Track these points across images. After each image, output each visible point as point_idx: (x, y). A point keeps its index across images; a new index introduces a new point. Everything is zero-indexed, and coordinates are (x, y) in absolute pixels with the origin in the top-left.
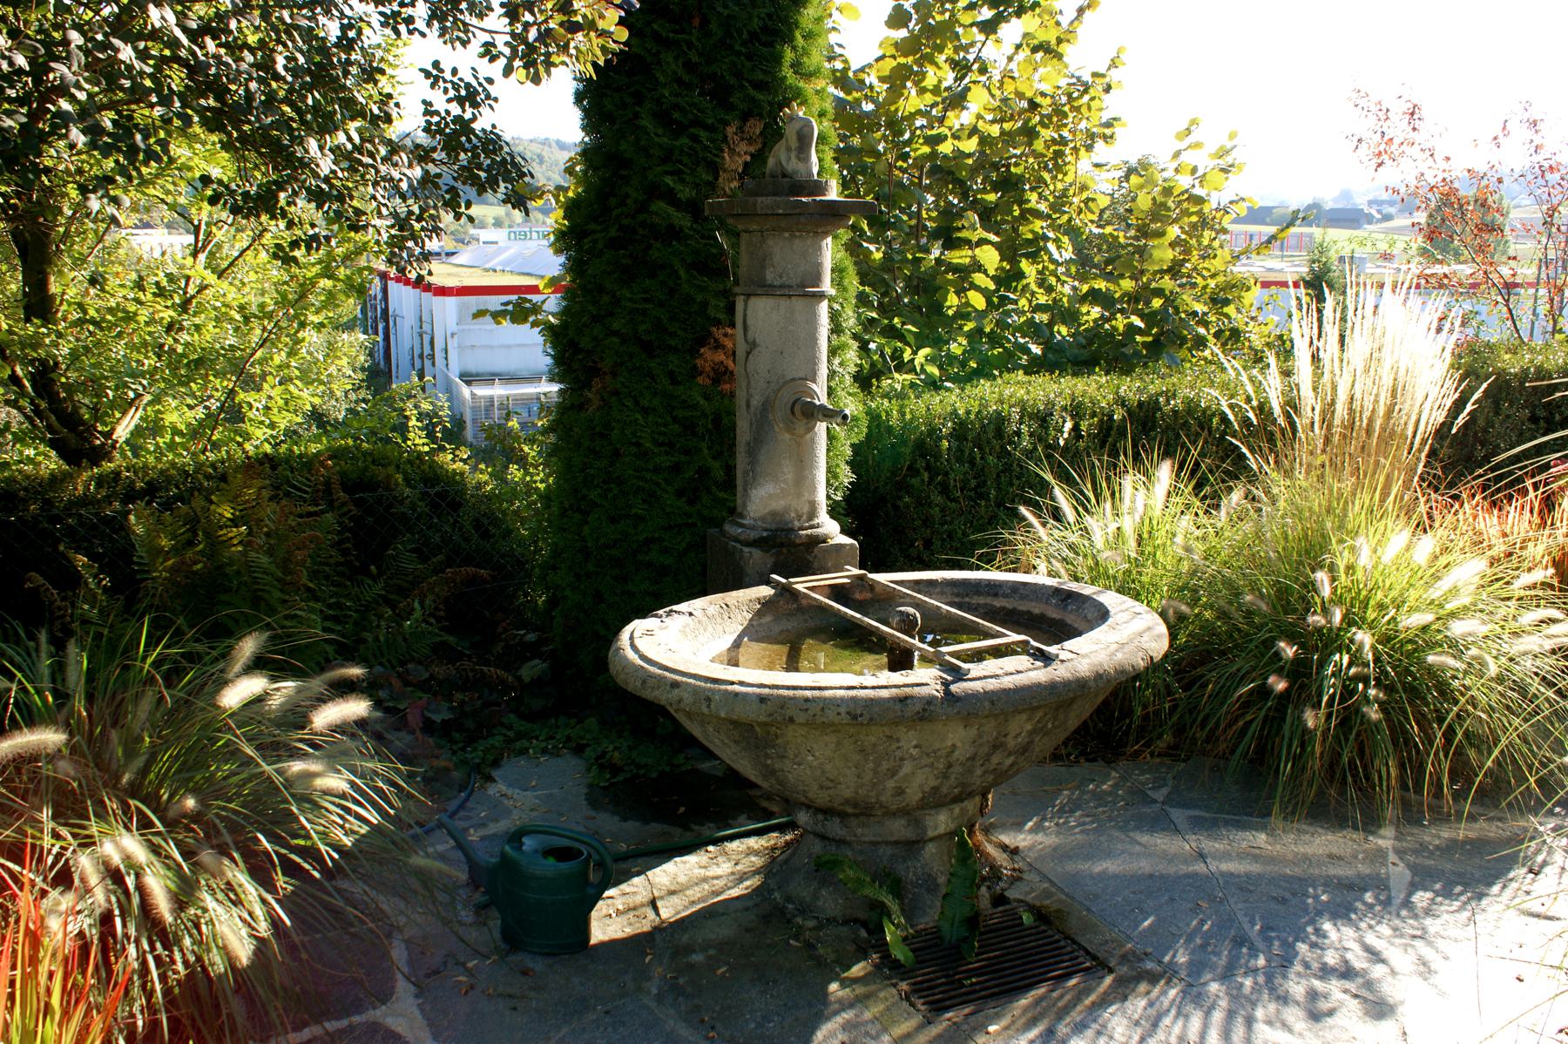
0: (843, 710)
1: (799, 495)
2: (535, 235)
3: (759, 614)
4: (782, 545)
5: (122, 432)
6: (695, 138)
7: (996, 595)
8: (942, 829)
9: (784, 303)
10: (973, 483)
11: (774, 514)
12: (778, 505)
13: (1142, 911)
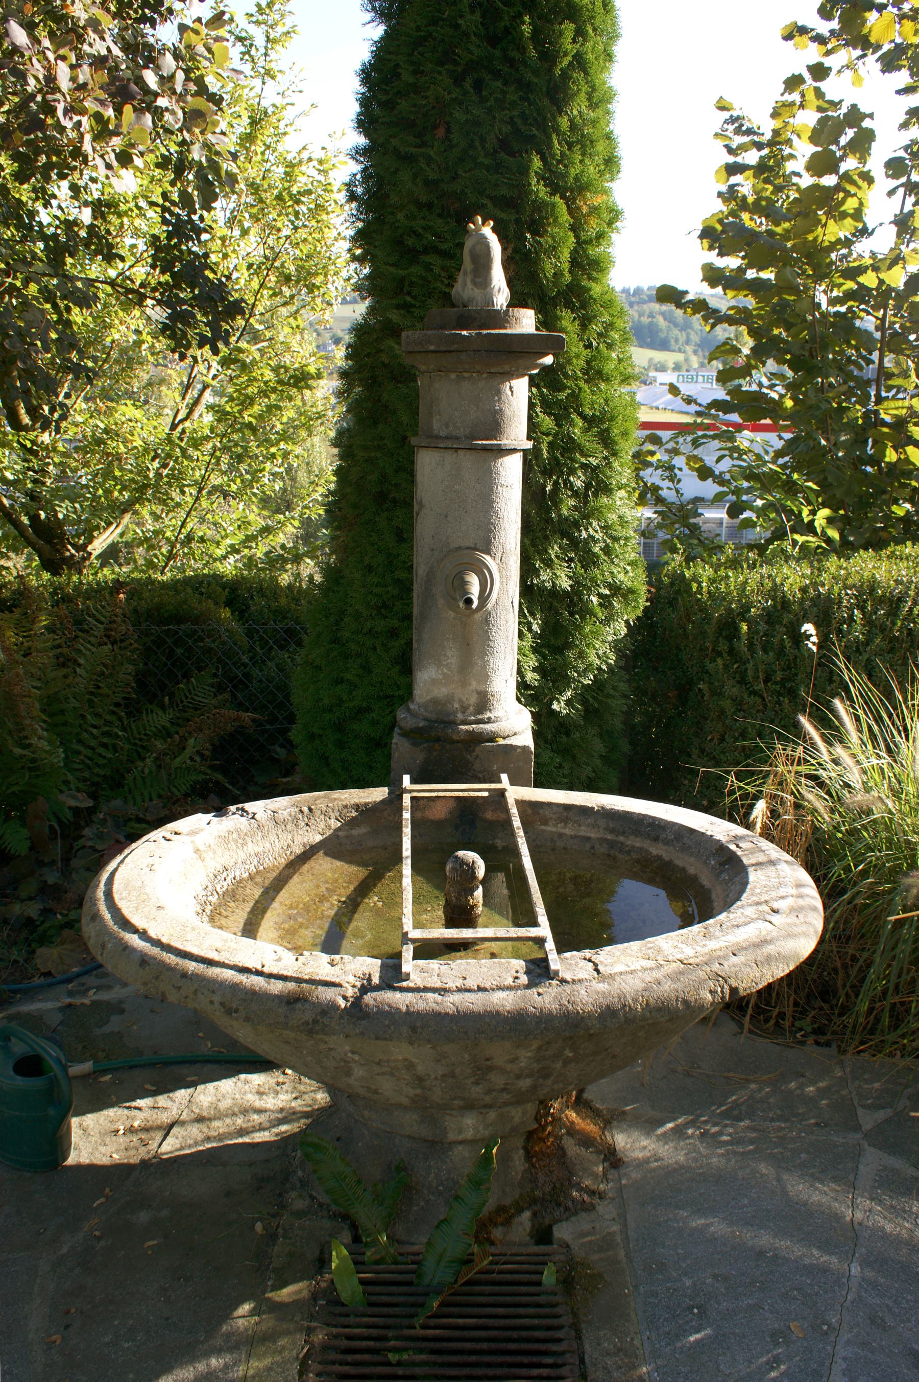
0: (217, 998)
1: (464, 684)
2: (700, 379)
3: (351, 824)
4: (438, 740)
5: (98, 545)
6: (428, 267)
7: (656, 839)
8: (469, 1134)
9: (449, 457)
10: (779, 676)
11: (435, 702)
12: (440, 692)
13: (703, 1313)
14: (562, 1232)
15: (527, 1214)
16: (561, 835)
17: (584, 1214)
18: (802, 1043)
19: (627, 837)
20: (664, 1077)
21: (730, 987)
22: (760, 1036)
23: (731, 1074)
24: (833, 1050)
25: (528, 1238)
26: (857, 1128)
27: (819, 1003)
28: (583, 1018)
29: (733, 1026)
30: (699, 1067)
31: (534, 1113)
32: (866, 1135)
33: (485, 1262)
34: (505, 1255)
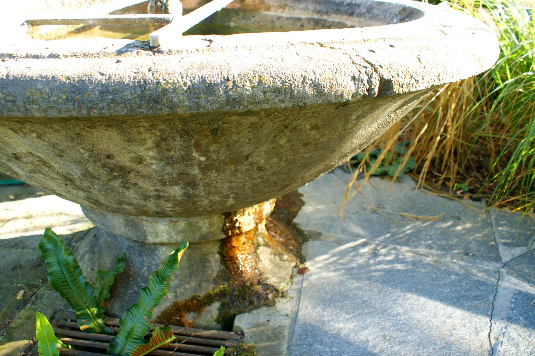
14: (242, 322)
15: (216, 305)
16: (279, 18)
17: (265, 308)
18: (461, 198)
19: (329, 16)
20: (357, 212)
21: (382, 79)
22: (431, 191)
23: (406, 214)
24: (483, 204)
25: (215, 323)
26: (498, 259)
27: (475, 173)
28: (165, 90)
29: (412, 183)
30: (383, 207)
31: (221, 225)
32: (505, 265)
33: (169, 340)
34: (189, 336)
